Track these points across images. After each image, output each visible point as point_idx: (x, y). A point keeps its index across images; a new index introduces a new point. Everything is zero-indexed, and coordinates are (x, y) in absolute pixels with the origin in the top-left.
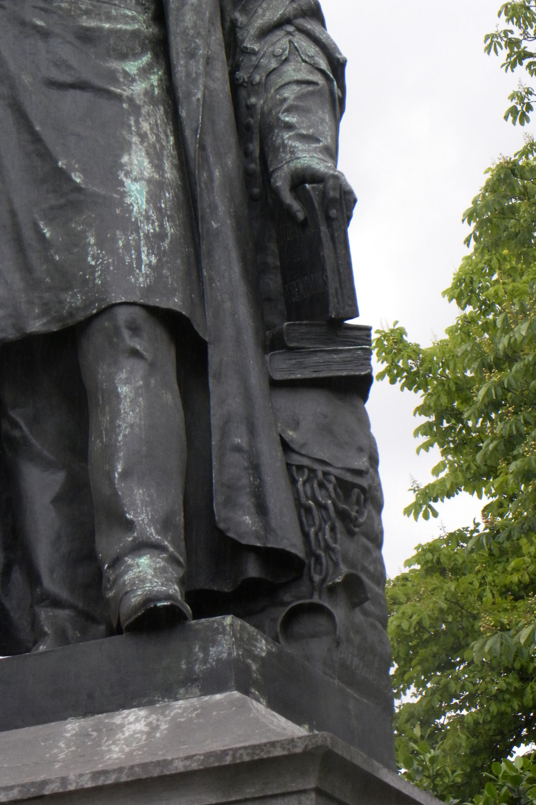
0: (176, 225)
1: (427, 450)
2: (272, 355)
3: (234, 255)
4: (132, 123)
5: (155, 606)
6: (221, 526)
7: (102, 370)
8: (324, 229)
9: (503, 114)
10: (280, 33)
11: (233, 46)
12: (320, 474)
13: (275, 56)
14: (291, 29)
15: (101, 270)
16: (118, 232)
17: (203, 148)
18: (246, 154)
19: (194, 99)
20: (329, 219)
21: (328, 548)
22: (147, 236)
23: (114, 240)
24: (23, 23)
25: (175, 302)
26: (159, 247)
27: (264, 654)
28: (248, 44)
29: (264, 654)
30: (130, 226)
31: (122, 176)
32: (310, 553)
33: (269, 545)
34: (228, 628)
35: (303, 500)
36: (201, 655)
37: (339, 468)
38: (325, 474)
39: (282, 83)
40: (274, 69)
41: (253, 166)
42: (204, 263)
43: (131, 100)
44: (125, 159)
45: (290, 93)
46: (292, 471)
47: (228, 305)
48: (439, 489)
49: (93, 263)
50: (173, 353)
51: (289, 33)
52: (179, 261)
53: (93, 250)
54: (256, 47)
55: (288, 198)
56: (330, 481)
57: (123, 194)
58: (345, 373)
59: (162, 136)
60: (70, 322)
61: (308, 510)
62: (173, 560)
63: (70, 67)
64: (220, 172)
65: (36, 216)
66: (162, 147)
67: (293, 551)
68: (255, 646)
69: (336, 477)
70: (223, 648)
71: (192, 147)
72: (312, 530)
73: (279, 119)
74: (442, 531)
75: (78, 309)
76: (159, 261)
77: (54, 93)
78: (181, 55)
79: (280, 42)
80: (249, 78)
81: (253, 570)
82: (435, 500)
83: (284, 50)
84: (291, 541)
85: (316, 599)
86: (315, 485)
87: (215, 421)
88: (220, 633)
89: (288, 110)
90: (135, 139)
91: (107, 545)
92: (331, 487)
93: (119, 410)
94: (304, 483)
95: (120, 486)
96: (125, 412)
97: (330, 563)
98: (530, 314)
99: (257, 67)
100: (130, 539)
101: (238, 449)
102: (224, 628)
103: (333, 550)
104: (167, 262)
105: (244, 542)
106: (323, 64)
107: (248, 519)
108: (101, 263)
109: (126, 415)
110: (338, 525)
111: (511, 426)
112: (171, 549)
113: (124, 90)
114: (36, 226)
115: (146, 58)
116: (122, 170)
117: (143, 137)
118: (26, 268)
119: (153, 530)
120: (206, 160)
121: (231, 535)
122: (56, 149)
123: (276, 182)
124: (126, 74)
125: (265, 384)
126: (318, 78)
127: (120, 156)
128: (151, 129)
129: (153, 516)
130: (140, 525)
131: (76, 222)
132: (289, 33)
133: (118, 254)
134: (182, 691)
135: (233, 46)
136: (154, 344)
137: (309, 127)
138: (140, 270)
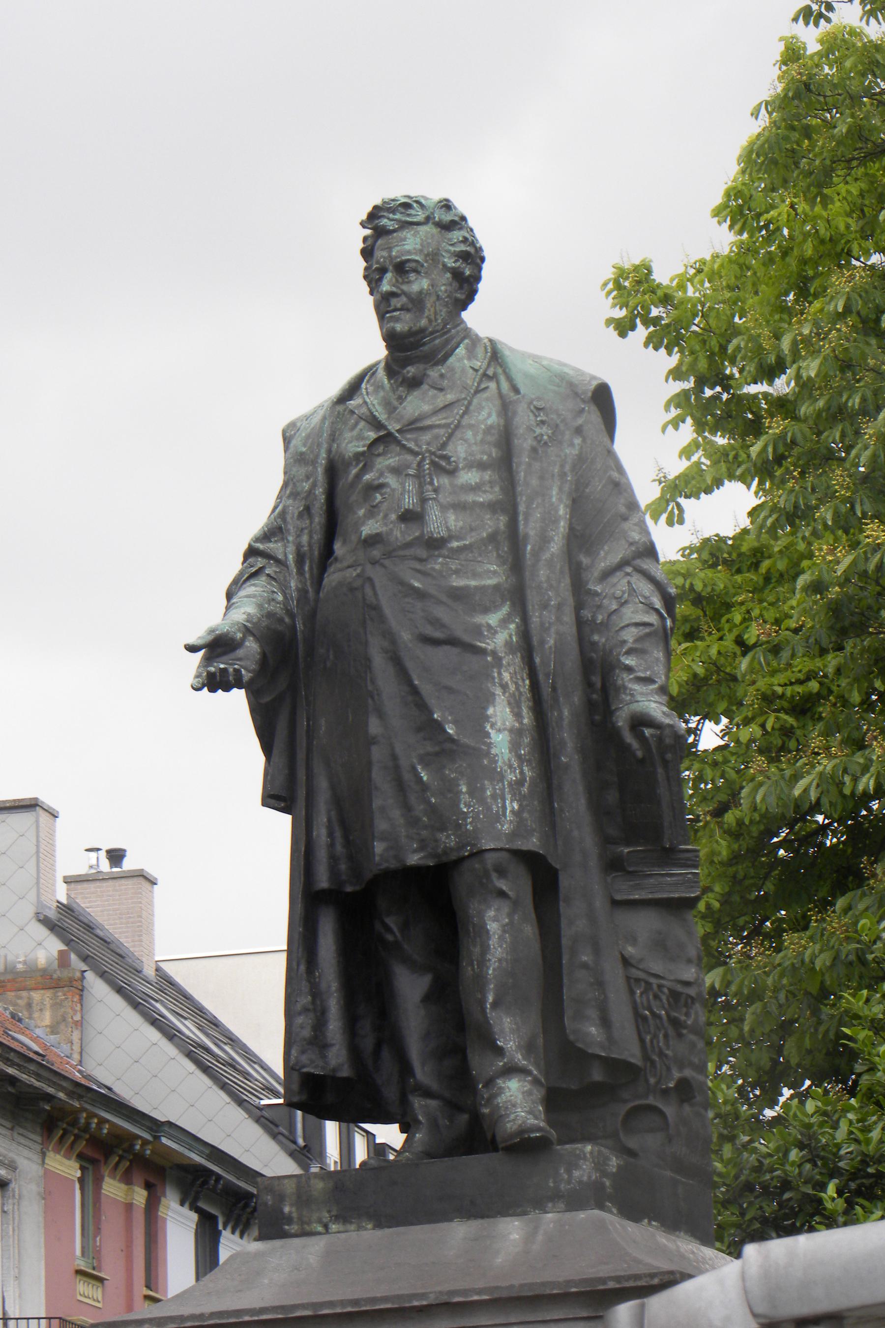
0: (533, 768)
1: (676, 428)
2: (614, 877)
3: (581, 788)
4: (496, 675)
5: (529, 1137)
6: (572, 1037)
7: (474, 907)
8: (660, 770)
9: (792, 16)
10: (619, 574)
11: (579, 587)
12: (655, 987)
13: (616, 598)
14: (629, 570)
15: (472, 817)
16: (486, 782)
17: (554, 689)
18: (589, 685)
19: (547, 646)
20: (665, 763)
21: (661, 1054)
22: (510, 784)
23: (483, 789)
24: (402, 583)
25: (533, 843)
26: (520, 793)
27: (614, 1170)
28: (591, 586)
29: (614, 1170)
31: (488, 728)
32: (646, 1057)
34: (588, 1155)
35: (641, 1010)
36: (566, 1176)
37: (671, 981)
38: (660, 986)
39: (623, 625)
40: (615, 610)
41: (595, 696)
43: (494, 653)
44: (490, 711)
45: (630, 636)
46: (631, 982)
47: (576, 833)
48: (695, 486)
49: (465, 810)
50: (530, 883)
51: (628, 574)
52: (536, 803)
53: (465, 798)
54: (598, 589)
55: (628, 738)
57: (489, 746)
58: (677, 895)
59: (520, 683)
60: (444, 859)
61: (645, 1019)
62: (536, 1082)
63: (443, 626)
64: (567, 714)
65: (415, 761)
66: (521, 694)
67: (633, 1060)
68: (608, 1165)
69: (669, 989)
70: (584, 1172)
71: (546, 691)
72: (649, 1037)
73: (619, 661)
74: (694, 536)
75: (451, 849)
76: (520, 806)
77: (430, 650)
78: (536, 607)
79: (620, 584)
80: (592, 617)
81: (597, 1075)
82: (686, 497)
83: (624, 592)
84: (632, 1053)
85: (651, 1100)
86: (651, 997)
87: (565, 942)
89: (629, 652)
90: (498, 691)
91: (481, 1064)
92: (664, 998)
93: (489, 946)
94: (642, 994)
95: (491, 1014)
98: (824, 346)
99: (599, 607)
100: (501, 1064)
101: (585, 966)
102: (585, 1154)
103: (666, 1056)
104: (527, 805)
105: (590, 1051)
106: (658, 603)
107: (593, 1030)
108: (472, 811)
110: (671, 1032)
111: (796, 497)
112: (535, 1072)
113: (488, 644)
114: (414, 769)
115: (505, 609)
116: (488, 722)
117: (504, 687)
118: (407, 807)
119: (520, 1057)
120: (556, 700)
121: (580, 1045)
122: (432, 702)
123: (617, 722)
124: (489, 626)
126: (653, 618)
127: (485, 708)
128: (511, 678)
129: (519, 1043)
131: (450, 769)
132: (628, 574)
134: (550, 1205)
135: (579, 587)
136: (517, 884)
137: (646, 670)
138: (505, 818)
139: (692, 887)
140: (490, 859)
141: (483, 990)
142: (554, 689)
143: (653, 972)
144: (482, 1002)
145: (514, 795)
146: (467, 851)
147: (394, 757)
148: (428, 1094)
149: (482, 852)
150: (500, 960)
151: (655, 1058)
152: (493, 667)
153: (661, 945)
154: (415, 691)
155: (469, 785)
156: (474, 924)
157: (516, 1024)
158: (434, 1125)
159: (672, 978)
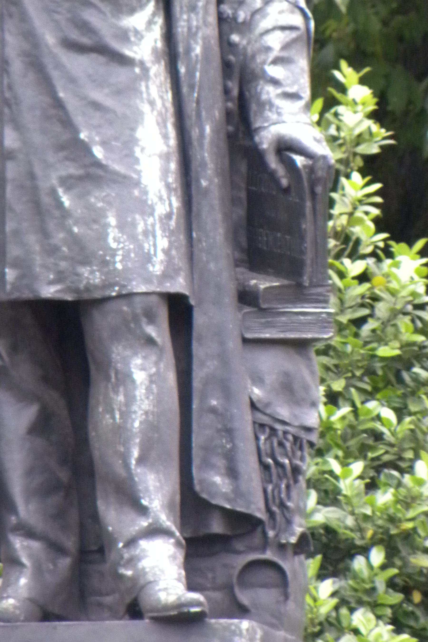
3: (219, 216)
7: (118, 352)
8: (308, 204)
19: (193, 54)
23: (134, 225)
25: (179, 285)
30: (146, 209)
33: (238, 509)
38: (285, 433)
42: (194, 226)
43: (142, 63)
45: (275, 41)
55: (273, 162)
56: (287, 439)
60: (86, 296)
62: (178, 544)
64: (207, 131)
71: (190, 107)
73: (264, 72)
75: (96, 287)
78: (185, 9)
80: (233, 14)
81: (217, 527)
85: (269, 555)
86: (275, 444)
88: (237, 635)
89: (276, 61)
90: (146, 108)
92: (288, 445)
93: (134, 397)
94: (266, 440)
96: (141, 400)
97: (284, 520)
101: (213, 410)
102: (241, 631)
103: (287, 508)
104: (175, 241)
105: (214, 502)
107: (218, 479)
108: (123, 248)
109: (141, 402)
112: (178, 534)
113: (135, 52)
114: (53, 193)
116: (138, 145)
117: (152, 103)
120: (199, 115)
121: (204, 496)
122: (78, 119)
123: (261, 143)
125: (239, 341)
130: (154, 512)
131: (96, 198)
133: (138, 240)
139: (325, 327)
140: (139, 304)
141: (126, 443)
142: (198, 102)
143: (280, 418)
144: (125, 458)
145: (164, 231)
146: (114, 291)
147: (32, 176)
148: (29, 533)
149: (130, 295)
150: (146, 413)
151: (275, 509)
152: (141, 80)
153: (289, 389)
154: (59, 104)
155: (120, 217)
156: (117, 372)
157: (160, 481)
158: (38, 571)
159: (297, 424)
